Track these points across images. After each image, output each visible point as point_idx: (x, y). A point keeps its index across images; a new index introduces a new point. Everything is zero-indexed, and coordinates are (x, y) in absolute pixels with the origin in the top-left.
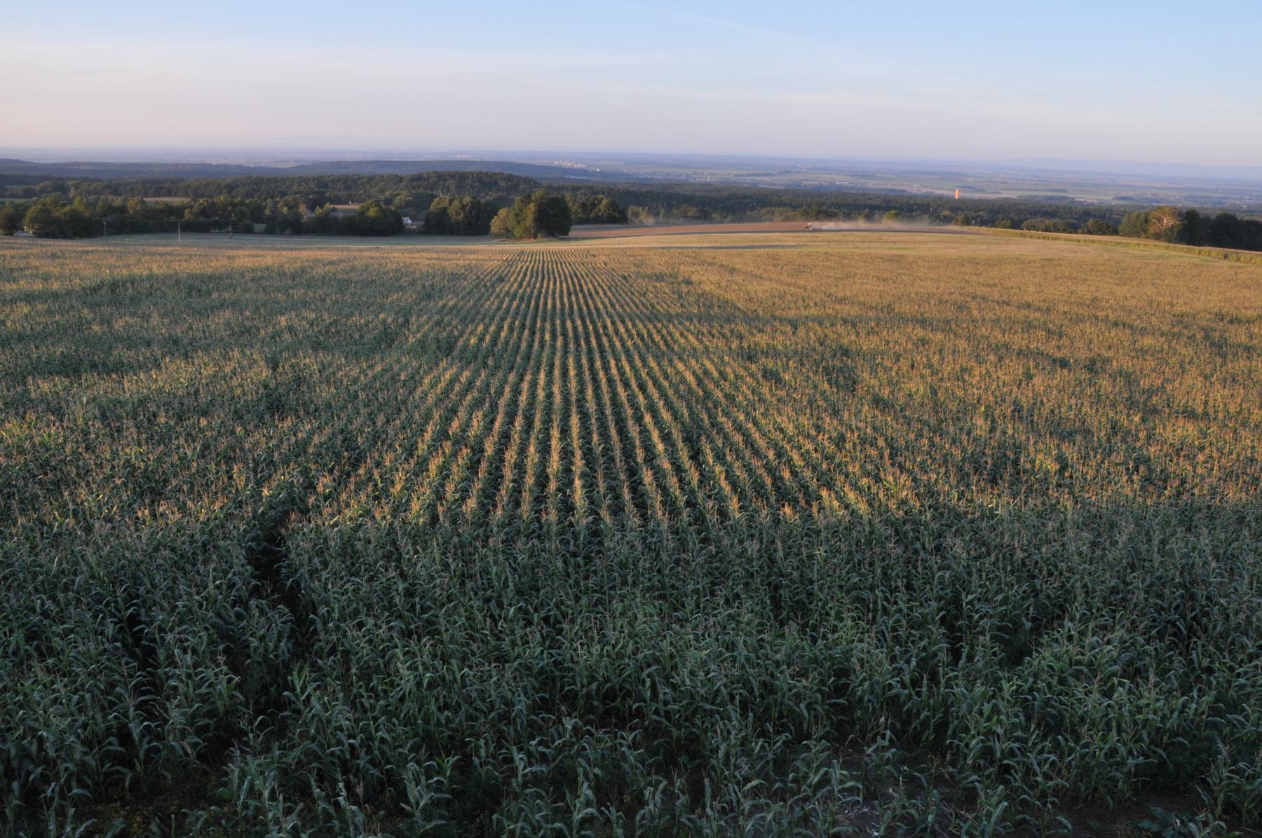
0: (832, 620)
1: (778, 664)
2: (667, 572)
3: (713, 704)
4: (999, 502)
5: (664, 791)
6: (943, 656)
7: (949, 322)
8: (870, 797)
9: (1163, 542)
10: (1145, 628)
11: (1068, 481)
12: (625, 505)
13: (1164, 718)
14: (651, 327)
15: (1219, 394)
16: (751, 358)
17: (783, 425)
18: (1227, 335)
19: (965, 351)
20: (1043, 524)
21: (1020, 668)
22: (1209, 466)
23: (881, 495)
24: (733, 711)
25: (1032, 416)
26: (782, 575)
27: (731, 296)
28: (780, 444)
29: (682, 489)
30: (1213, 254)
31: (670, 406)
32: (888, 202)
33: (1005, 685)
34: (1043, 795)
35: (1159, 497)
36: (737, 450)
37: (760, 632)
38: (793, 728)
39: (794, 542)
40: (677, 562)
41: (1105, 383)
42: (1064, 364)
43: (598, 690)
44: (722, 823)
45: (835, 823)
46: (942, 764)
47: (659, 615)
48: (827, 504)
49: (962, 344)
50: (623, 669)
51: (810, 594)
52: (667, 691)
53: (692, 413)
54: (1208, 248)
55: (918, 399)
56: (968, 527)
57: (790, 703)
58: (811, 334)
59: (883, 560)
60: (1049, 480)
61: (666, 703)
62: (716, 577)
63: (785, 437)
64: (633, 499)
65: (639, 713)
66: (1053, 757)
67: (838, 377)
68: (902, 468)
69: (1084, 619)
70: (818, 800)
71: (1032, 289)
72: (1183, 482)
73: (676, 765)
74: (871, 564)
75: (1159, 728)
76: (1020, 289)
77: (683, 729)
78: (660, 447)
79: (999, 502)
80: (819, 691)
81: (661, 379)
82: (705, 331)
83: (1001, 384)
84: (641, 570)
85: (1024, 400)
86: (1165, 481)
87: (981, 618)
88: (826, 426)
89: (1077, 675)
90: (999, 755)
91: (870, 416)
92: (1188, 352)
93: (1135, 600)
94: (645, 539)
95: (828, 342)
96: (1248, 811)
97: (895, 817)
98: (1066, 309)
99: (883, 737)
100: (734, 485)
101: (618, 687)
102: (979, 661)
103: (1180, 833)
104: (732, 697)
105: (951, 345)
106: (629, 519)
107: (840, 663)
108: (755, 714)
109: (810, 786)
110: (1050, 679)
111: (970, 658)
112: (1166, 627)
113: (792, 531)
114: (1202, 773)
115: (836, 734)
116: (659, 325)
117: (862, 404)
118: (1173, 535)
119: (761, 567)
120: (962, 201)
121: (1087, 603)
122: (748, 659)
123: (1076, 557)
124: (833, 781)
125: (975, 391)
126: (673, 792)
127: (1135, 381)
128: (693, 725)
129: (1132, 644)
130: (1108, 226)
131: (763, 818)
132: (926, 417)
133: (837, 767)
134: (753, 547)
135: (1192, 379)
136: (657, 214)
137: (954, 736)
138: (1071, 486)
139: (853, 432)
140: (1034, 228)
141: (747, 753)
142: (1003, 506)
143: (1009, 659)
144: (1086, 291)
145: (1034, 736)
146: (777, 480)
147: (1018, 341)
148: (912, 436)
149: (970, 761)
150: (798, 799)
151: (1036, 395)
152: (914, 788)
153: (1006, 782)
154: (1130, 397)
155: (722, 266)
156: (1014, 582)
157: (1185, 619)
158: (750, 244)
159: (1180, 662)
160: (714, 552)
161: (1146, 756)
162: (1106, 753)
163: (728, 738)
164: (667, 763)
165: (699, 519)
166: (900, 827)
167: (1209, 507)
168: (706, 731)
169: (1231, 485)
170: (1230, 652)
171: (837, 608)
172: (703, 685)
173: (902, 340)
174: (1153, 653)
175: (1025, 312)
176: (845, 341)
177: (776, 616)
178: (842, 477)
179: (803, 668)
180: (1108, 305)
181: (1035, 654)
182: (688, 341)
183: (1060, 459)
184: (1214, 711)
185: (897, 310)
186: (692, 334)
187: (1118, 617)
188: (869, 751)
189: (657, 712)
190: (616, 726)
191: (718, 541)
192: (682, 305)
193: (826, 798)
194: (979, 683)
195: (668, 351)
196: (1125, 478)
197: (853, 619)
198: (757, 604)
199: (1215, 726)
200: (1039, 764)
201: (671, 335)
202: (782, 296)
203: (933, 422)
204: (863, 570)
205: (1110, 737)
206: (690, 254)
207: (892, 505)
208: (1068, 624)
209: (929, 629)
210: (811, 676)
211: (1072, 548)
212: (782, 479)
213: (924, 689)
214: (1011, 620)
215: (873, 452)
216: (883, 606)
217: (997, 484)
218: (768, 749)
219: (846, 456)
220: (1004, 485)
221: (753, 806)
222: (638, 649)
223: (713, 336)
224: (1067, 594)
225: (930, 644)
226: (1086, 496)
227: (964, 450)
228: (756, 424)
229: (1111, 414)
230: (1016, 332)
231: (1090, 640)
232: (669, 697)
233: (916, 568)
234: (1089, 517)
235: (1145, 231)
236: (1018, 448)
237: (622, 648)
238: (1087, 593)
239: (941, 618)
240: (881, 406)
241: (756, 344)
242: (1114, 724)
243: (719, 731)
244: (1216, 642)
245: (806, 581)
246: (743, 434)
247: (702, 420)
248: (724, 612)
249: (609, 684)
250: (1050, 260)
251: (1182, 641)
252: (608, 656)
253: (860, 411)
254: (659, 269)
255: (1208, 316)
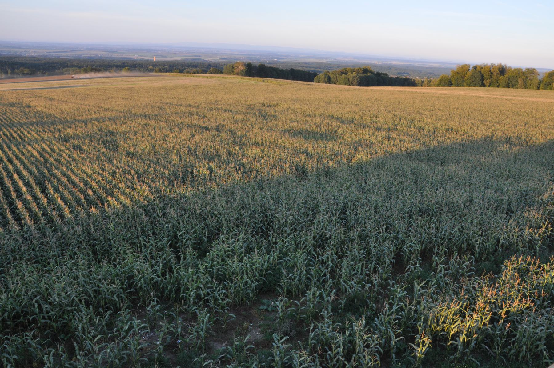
0: (122, 255)
1: (100, 280)
2: (37, 249)
3: (72, 306)
4: (187, 191)
5: (54, 355)
6: (173, 261)
7: (157, 115)
8: (152, 328)
9: (253, 197)
10: (251, 232)
11: (214, 177)
12: (9, 221)
13: (263, 265)
14: (11, 130)
15: (266, 135)
16: (66, 141)
17: (86, 170)
18: (267, 112)
19: (165, 127)
20: (206, 197)
21: (206, 258)
22: (266, 164)
23: (136, 196)
24: (83, 307)
25: (196, 152)
26: (95, 240)
27: (52, 112)
28: (86, 179)
29: (39, 208)
30: (259, 80)
31: (26, 168)
32: (124, 63)
33: (201, 267)
34: (223, 307)
35: (249, 179)
36: (65, 185)
37: (89, 268)
38: (112, 308)
39: (98, 223)
40: (42, 243)
41: (224, 135)
42: (207, 129)
43: (9, 316)
44: (86, 360)
45: (139, 344)
46: (181, 306)
47: (36, 271)
48: (111, 203)
49: (163, 125)
50: (21, 302)
51: (110, 246)
52: (47, 306)
53: (39, 171)
54: (256, 78)
55: (146, 150)
56: (175, 204)
57: (109, 297)
58: (94, 126)
59: (141, 224)
60: (206, 178)
61: (48, 312)
62: (63, 246)
63: (87, 176)
64: (13, 217)
65: (35, 321)
66: (224, 291)
67: (109, 145)
68: (143, 182)
69: (228, 233)
70: (129, 337)
71: (190, 98)
72: (257, 171)
73: (58, 340)
74: (136, 227)
75: (261, 269)
76: (185, 99)
77: (59, 322)
78: (24, 189)
79: (187, 191)
80: (121, 288)
81: (20, 156)
82: (41, 130)
83: (182, 140)
84: (23, 251)
85: (192, 146)
86: (251, 172)
87: (187, 241)
88: (107, 168)
89: (228, 256)
90: (203, 296)
91: (126, 161)
92: (253, 119)
93: (245, 222)
94: (23, 236)
95: (103, 129)
96: (295, 291)
97: (165, 333)
98: (205, 106)
99: (153, 301)
100: (66, 202)
101: (20, 311)
102: (189, 259)
103: (274, 307)
104: (81, 301)
105: (158, 125)
106: (12, 227)
107: (129, 273)
108: (93, 306)
109: (125, 331)
110: (218, 260)
111: (185, 259)
112: (258, 230)
113: (97, 219)
114: (278, 282)
115: (132, 305)
116: (16, 129)
117: (122, 156)
118: (256, 193)
119: (85, 238)
120: (157, 62)
121: (228, 226)
122: (85, 282)
123: (221, 208)
124: (135, 326)
125: (171, 144)
126: (59, 354)
127: (235, 133)
128: (64, 319)
129: (247, 239)
130: (218, 71)
131: (106, 352)
132: (151, 158)
133: (135, 319)
134: (79, 229)
135: (256, 130)
136: (7, 73)
137: (184, 293)
138: (215, 180)
139: (119, 169)
140: (189, 72)
141: (93, 325)
142: (189, 192)
143: (200, 255)
144: (212, 98)
145: (215, 285)
146: (86, 196)
147: (187, 121)
148: (146, 167)
149: (191, 302)
150: (121, 339)
151: (196, 143)
152: (171, 319)
153: (207, 306)
154: (234, 140)
155: (46, 97)
156: (198, 223)
157: (265, 225)
158: (59, 86)
159: (265, 242)
160: (60, 235)
161: (258, 281)
162: (244, 284)
163: (82, 320)
164: (53, 341)
165: (50, 221)
166: (168, 337)
167: (268, 180)
168: (71, 320)
169: (275, 170)
170: (282, 234)
171: (123, 249)
172: (65, 299)
173: (137, 125)
174: (255, 241)
175: (189, 108)
176: (111, 128)
177: (96, 259)
178: (117, 190)
179: (112, 279)
180: (221, 103)
181: (211, 251)
182: (33, 136)
183: (210, 169)
184: (279, 258)
185: (133, 112)
186: (34, 132)
187: (240, 230)
188: (148, 309)
189: (44, 318)
190: (22, 331)
191: (61, 230)
192: (27, 118)
193: (133, 334)
194: (190, 268)
195: (22, 142)
196: (236, 173)
197: (132, 253)
198: (86, 255)
199: (280, 263)
200: (219, 296)
201: (22, 133)
202: (78, 110)
203: (154, 160)
204: (132, 230)
205: (244, 277)
206: (28, 92)
207: (141, 199)
208: (221, 236)
209: (166, 250)
210: (116, 282)
211: (219, 205)
212: (89, 195)
213: (168, 276)
214: (199, 239)
215: (129, 177)
216: (144, 244)
217: (185, 183)
218: (102, 320)
219: (117, 180)
220: (188, 183)
221: (99, 348)
222: (28, 290)
223: (45, 132)
224: (220, 224)
225: (167, 256)
226: (222, 182)
227: (169, 171)
228: (72, 171)
229: (228, 148)
230: (186, 117)
231: (231, 241)
232: (48, 309)
233: (155, 225)
234: (224, 191)
235: (233, 72)
236: (192, 167)
237: (19, 291)
238: (227, 222)
239: (170, 245)
240: (130, 156)
241: (68, 134)
242: (245, 272)
243: (77, 319)
244: (277, 232)
245: (107, 240)
246: (67, 177)
247: (45, 173)
248: (70, 262)
249: (15, 311)
250: (196, 86)
251: (264, 234)
252: (12, 297)
253: (121, 159)
254: (11, 101)
255: (259, 105)
